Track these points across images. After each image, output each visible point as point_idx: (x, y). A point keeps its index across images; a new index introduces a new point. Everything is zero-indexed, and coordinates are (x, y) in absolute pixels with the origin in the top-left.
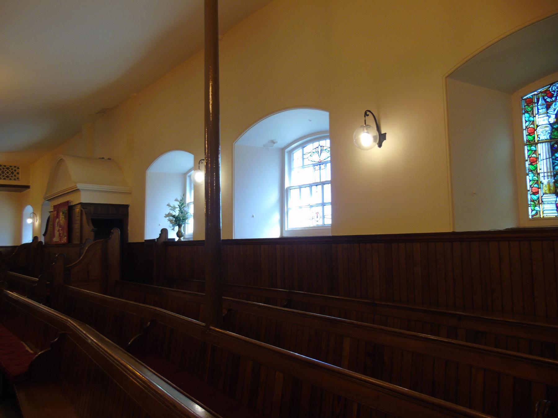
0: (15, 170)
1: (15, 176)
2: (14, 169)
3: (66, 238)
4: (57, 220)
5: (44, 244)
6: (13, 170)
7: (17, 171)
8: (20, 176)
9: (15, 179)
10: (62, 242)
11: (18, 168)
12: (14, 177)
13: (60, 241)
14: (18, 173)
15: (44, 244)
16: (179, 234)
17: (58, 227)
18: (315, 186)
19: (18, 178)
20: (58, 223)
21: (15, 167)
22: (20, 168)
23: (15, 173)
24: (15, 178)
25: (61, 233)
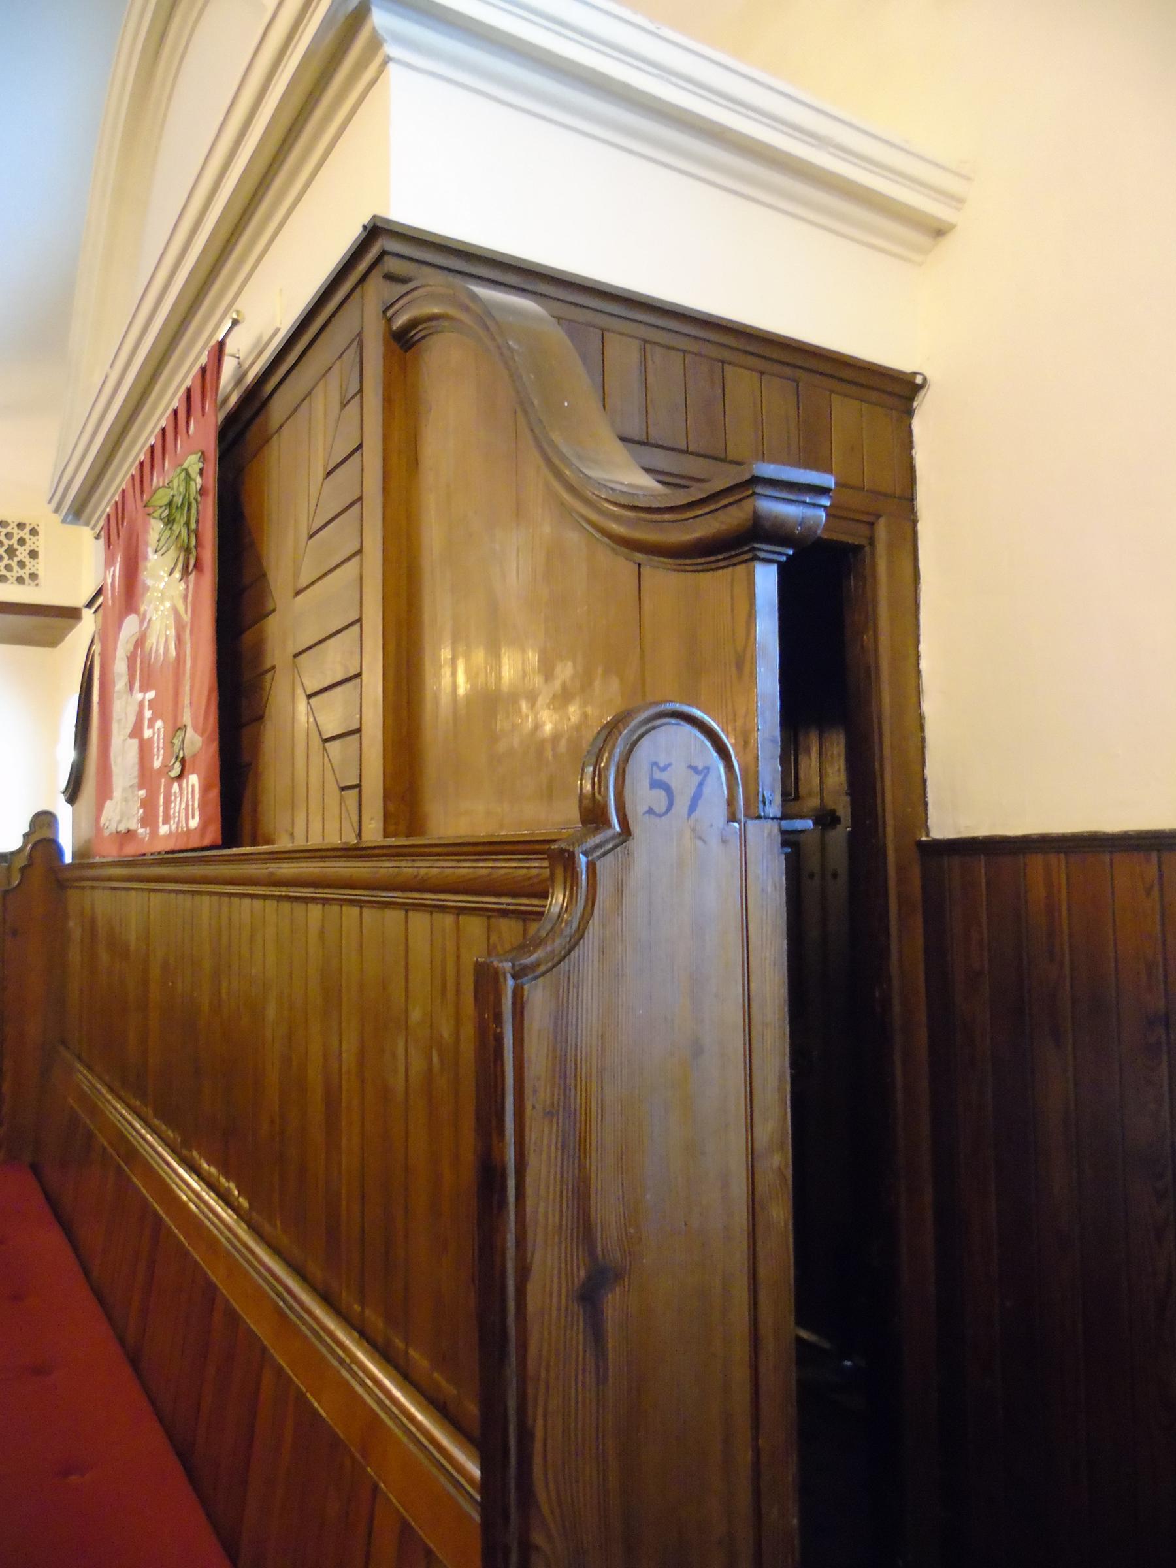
0: (22, 542)
1: (22, 564)
2: (18, 534)
3: (193, 779)
4: (131, 625)
5: (68, 859)
6: (14, 541)
7: (29, 542)
8: (40, 566)
9: (20, 580)
10: (164, 830)
11: (34, 532)
12: (17, 571)
13: (144, 821)
14: (33, 554)
15: (68, 859)
16: (465, 648)
17: (175, 793)
18: (756, 375)
19: (33, 576)
20: (131, 659)
21: (21, 526)
22: (41, 530)
23: (22, 553)
24: (21, 573)
25: (150, 740)
